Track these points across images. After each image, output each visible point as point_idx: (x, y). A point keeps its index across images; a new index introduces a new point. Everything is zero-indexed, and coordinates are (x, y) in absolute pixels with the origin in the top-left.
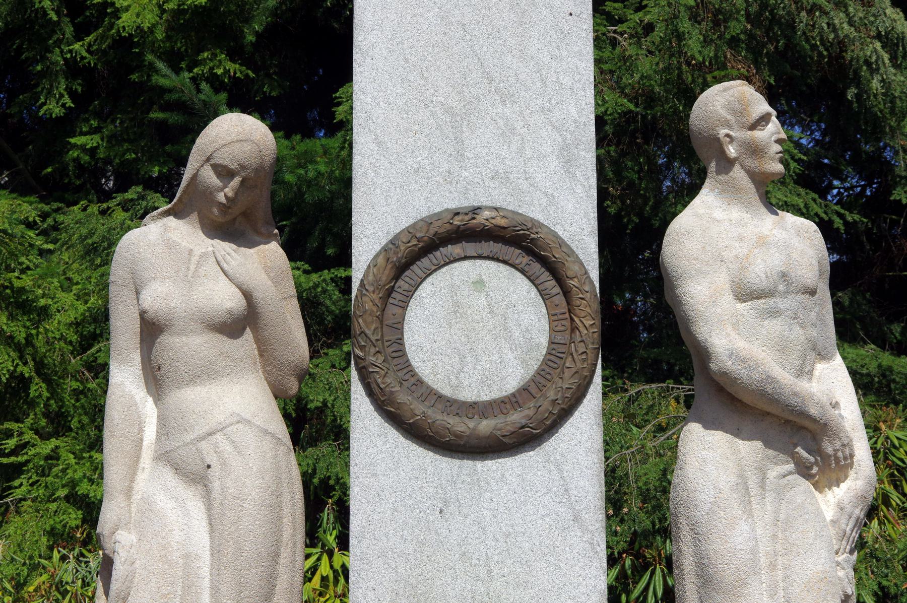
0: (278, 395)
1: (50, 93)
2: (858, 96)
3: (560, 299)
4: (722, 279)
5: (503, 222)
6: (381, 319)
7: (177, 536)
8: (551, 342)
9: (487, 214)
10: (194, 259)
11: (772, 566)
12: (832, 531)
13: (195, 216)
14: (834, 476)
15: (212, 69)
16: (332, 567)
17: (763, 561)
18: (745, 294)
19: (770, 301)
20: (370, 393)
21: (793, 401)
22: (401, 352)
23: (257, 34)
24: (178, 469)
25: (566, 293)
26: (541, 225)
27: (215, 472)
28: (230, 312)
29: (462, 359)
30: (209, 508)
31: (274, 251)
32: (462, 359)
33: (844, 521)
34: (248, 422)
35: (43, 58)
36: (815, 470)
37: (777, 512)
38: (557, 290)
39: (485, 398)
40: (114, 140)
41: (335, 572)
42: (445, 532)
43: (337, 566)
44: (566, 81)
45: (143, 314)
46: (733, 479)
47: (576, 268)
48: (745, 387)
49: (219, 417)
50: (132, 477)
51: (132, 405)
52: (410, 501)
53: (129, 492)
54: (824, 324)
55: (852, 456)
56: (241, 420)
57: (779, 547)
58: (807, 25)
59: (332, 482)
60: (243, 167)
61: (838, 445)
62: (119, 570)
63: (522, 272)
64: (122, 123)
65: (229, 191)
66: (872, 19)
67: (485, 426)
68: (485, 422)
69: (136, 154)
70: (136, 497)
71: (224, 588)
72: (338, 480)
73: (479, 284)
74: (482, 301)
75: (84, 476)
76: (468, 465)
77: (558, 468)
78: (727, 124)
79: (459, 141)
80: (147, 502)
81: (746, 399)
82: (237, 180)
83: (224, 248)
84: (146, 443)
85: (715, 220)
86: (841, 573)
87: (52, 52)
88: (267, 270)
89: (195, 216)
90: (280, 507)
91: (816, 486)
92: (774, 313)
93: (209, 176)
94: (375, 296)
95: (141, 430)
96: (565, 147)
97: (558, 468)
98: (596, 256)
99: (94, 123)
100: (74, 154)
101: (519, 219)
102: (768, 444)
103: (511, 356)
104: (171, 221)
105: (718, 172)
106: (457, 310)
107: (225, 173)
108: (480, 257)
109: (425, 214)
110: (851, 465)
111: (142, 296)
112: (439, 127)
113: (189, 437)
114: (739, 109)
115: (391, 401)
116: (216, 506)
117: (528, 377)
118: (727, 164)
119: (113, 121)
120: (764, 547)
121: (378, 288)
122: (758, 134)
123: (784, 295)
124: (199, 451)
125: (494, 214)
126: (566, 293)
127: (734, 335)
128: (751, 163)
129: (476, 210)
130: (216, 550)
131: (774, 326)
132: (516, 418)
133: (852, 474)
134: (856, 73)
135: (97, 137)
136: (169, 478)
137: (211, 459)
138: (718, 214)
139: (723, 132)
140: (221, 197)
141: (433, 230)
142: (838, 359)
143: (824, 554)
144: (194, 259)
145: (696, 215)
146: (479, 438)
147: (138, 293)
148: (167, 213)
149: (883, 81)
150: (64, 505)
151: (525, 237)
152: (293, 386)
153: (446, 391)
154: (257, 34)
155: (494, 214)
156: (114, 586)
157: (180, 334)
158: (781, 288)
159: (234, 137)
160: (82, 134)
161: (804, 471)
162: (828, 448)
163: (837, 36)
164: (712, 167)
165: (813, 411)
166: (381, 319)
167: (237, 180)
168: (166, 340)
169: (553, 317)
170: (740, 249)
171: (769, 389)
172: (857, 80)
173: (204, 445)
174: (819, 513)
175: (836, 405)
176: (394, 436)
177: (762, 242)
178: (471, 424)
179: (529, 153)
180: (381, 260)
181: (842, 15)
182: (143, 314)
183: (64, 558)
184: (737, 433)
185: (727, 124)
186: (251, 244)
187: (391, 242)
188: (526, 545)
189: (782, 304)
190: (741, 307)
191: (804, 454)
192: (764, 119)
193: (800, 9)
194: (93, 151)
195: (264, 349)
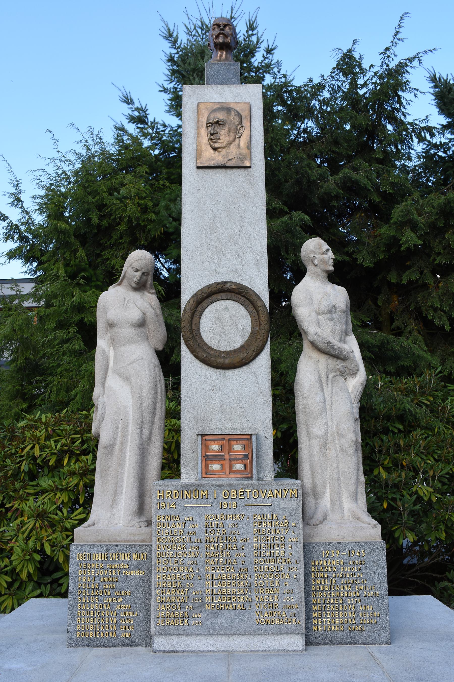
3: (256, 314)
9: (229, 284)
10: (126, 301)
28: (139, 320)
29: (221, 336)
37: (332, 389)
38: (254, 311)
44: (257, 237)
74: (227, 315)
77: (255, 375)
97: (255, 375)
98: (268, 299)
129: (226, 283)
142: (353, 336)
153: (215, 348)
169: (253, 321)
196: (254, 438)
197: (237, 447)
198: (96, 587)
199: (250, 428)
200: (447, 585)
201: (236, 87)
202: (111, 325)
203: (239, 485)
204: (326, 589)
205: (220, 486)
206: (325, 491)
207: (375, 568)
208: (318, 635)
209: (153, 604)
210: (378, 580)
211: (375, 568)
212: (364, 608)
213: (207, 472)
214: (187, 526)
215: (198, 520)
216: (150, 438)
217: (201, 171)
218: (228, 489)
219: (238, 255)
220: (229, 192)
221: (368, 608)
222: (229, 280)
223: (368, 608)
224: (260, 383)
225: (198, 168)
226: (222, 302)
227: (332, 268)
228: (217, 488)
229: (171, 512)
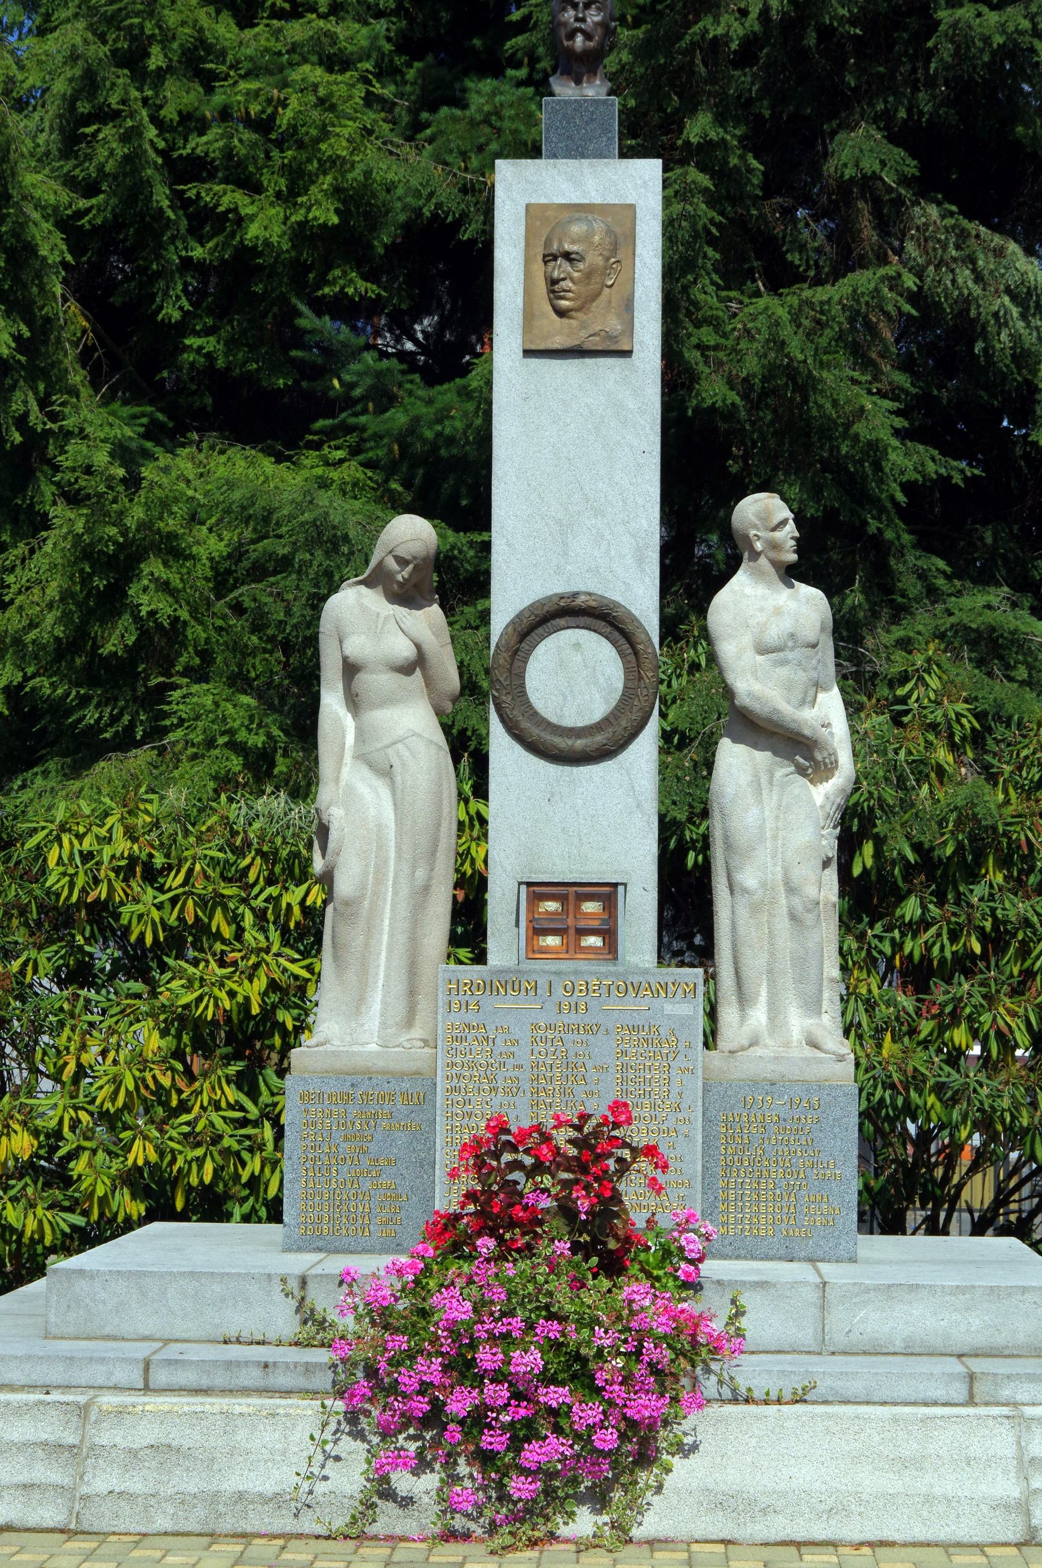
0: (439, 713)
1: (166, 294)
2: (985, 350)
3: (632, 658)
4: (747, 640)
5: (593, 604)
6: (510, 671)
7: (372, 812)
8: (625, 687)
9: (583, 598)
10: (381, 620)
11: (775, 838)
12: (821, 813)
13: (380, 588)
14: (824, 775)
15: (343, 288)
16: (468, 813)
17: (768, 834)
18: (763, 650)
19: (781, 654)
20: (503, 720)
21: (792, 726)
22: (523, 693)
23: (386, 246)
24: (372, 766)
25: (636, 653)
26: (620, 605)
27: (397, 770)
28: (406, 659)
29: (565, 698)
30: (394, 793)
31: (435, 610)
32: (565, 698)
33: (828, 807)
34: (419, 736)
35: (159, 257)
36: (810, 771)
37: (780, 800)
38: (630, 651)
39: (580, 725)
40: (232, 344)
41: (471, 819)
42: (551, 814)
43: (472, 812)
44: (640, 501)
45: (345, 660)
46: (750, 778)
47: (643, 636)
48: (759, 717)
49: (400, 732)
50: (339, 770)
51: (338, 720)
52: (528, 793)
53: (337, 780)
54: (825, 665)
55: (836, 762)
56: (415, 734)
57: (780, 824)
58: (933, 280)
59: (469, 733)
60: (415, 558)
61: (826, 754)
62: (333, 835)
63: (607, 638)
64: (240, 324)
65: (406, 573)
66: (1003, 271)
67: (579, 744)
68: (579, 742)
69: (257, 363)
70: (342, 783)
71: (404, 847)
72: (474, 731)
73: (577, 646)
74: (579, 658)
75: (242, 725)
76: (567, 770)
77: (628, 774)
78: (756, 527)
79: (565, 544)
80: (350, 790)
81: (761, 724)
82: (411, 566)
83: (401, 611)
84: (347, 746)
85: (745, 595)
86: (824, 842)
87: (166, 249)
88: (431, 626)
89: (380, 588)
90: (441, 793)
91: (811, 781)
92: (784, 663)
93: (391, 564)
94: (505, 655)
95: (344, 737)
96: (638, 549)
97: (628, 774)
98: (657, 627)
99: (209, 321)
100: (189, 357)
101: (605, 602)
102: (775, 753)
103: (597, 696)
104: (363, 589)
105: (750, 560)
106: (562, 664)
107: (402, 562)
108: (578, 627)
109: (541, 596)
110: (837, 767)
111: (344, 646)
112: (551, 534)
113: (379, 745)
114: (764, 516)
115: (517, 727)
116: (399, 794)
117: (609, 710)
118: (755, 555)
119: (230, 322)
120: (770, 824)
121: (508, 650)
122: (778, 535)
123: (792, 649)
124: (387, 755)
125: (588, 598)
126: (636, 653)
127: (752, 681)
128: (772, 554)
129: (575, 595)
130: (399, 821)
131: (783, 672)
132: (599, 739)
133: (837, 773)
134: (984, 327)
135: (212, 339)
136: (365, 771)
137: (395, 761)
138: (748, 591)
139: (753, 532)
140: (399, 578)
141: (546, 608)
142: (836, 690)
143: (811, 829)
144: (381, 620)
145: (733, 591)
146: (574, 752)
147: (341, 642)
148: (360, 583)
149: (1010, 335)
150: (227, 752)
151: (609, 614)
152: (449, 707)
153: (554, 720)
154: (386, 246)
155: (588, 598)
156: (331, 845)
157: (373, 672)
158: (790, 644)
159: (409, 537)
160: (198, 334)
161: (802, 771)
162: (819, 757)
163: (961, 294)
164: (746, 555)
165: (807, 732)
166: (510, 671)
167: (411, 566)
168: (361, 677)
169: (627, 670)
170: (761, 618)
171: (775, 718)
172: (984, 334)
173: (390, 751)
174: (811, 800)
175: (827, 725)
176: (518, 748)
177: (778, 612)
178: (570, 742)
179: (613, 553)
180: (510, 629)
181: (968, 272)
182: (345, 660)
183: (231, 800)
184: (755, 746)
185: (756, 527)
186: (419, 607)
187: (517, 616)
188: (605, 823)
189: (790, 655)
190: (760, 659)
191: (801, 760)
192: (784, 523)
193: (929, 263)
194: (209, 356)
195: (429, 682)
196: (621, 889)
197: (591, 907)
198: (334, 1149)
199: (615, 872)
200: (264, 548)
201: (606, 165)
202: (351, 669)
203: (591, 973)
204: (746, 1163)
205: (558, 973)
206: (758, 994)
207: (836, 1130)
208: (726, 1242)
209: (437, 1172)
210: (841, 1151)
211: (836, 1130)
212: (812, 1199)
213: (533, 952)
214: (498, 1041)
215: (516, 1032)
216: (426, 889)
217: (534, 362)
218: (572, 978)
219: (602, 537)
220: (587, 405)
221: (819, 1198)
222: (583, 589)
223: (819, 1198)
224: (637, 788)
225: (528, 353)
226: (569, 631)
227: (793, 557)
228: (552, 978)
229: (472, 1018)
